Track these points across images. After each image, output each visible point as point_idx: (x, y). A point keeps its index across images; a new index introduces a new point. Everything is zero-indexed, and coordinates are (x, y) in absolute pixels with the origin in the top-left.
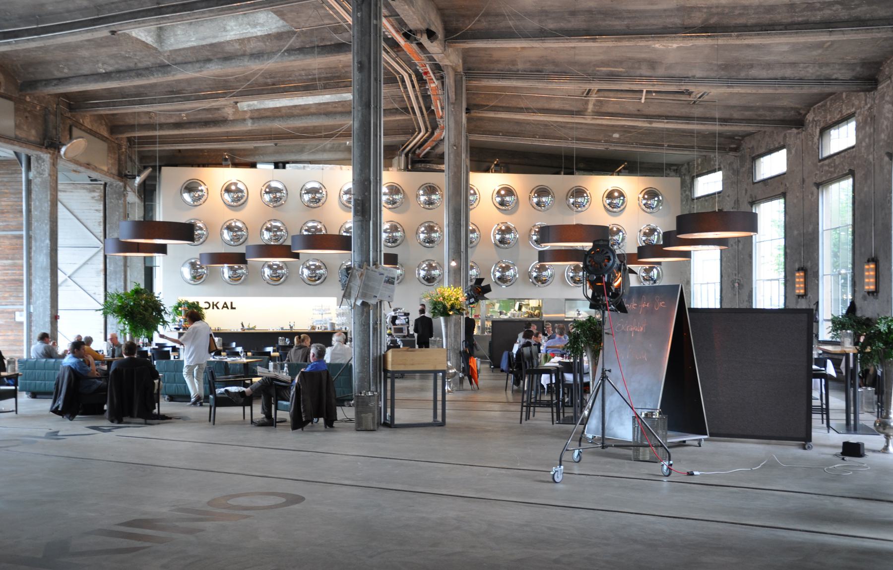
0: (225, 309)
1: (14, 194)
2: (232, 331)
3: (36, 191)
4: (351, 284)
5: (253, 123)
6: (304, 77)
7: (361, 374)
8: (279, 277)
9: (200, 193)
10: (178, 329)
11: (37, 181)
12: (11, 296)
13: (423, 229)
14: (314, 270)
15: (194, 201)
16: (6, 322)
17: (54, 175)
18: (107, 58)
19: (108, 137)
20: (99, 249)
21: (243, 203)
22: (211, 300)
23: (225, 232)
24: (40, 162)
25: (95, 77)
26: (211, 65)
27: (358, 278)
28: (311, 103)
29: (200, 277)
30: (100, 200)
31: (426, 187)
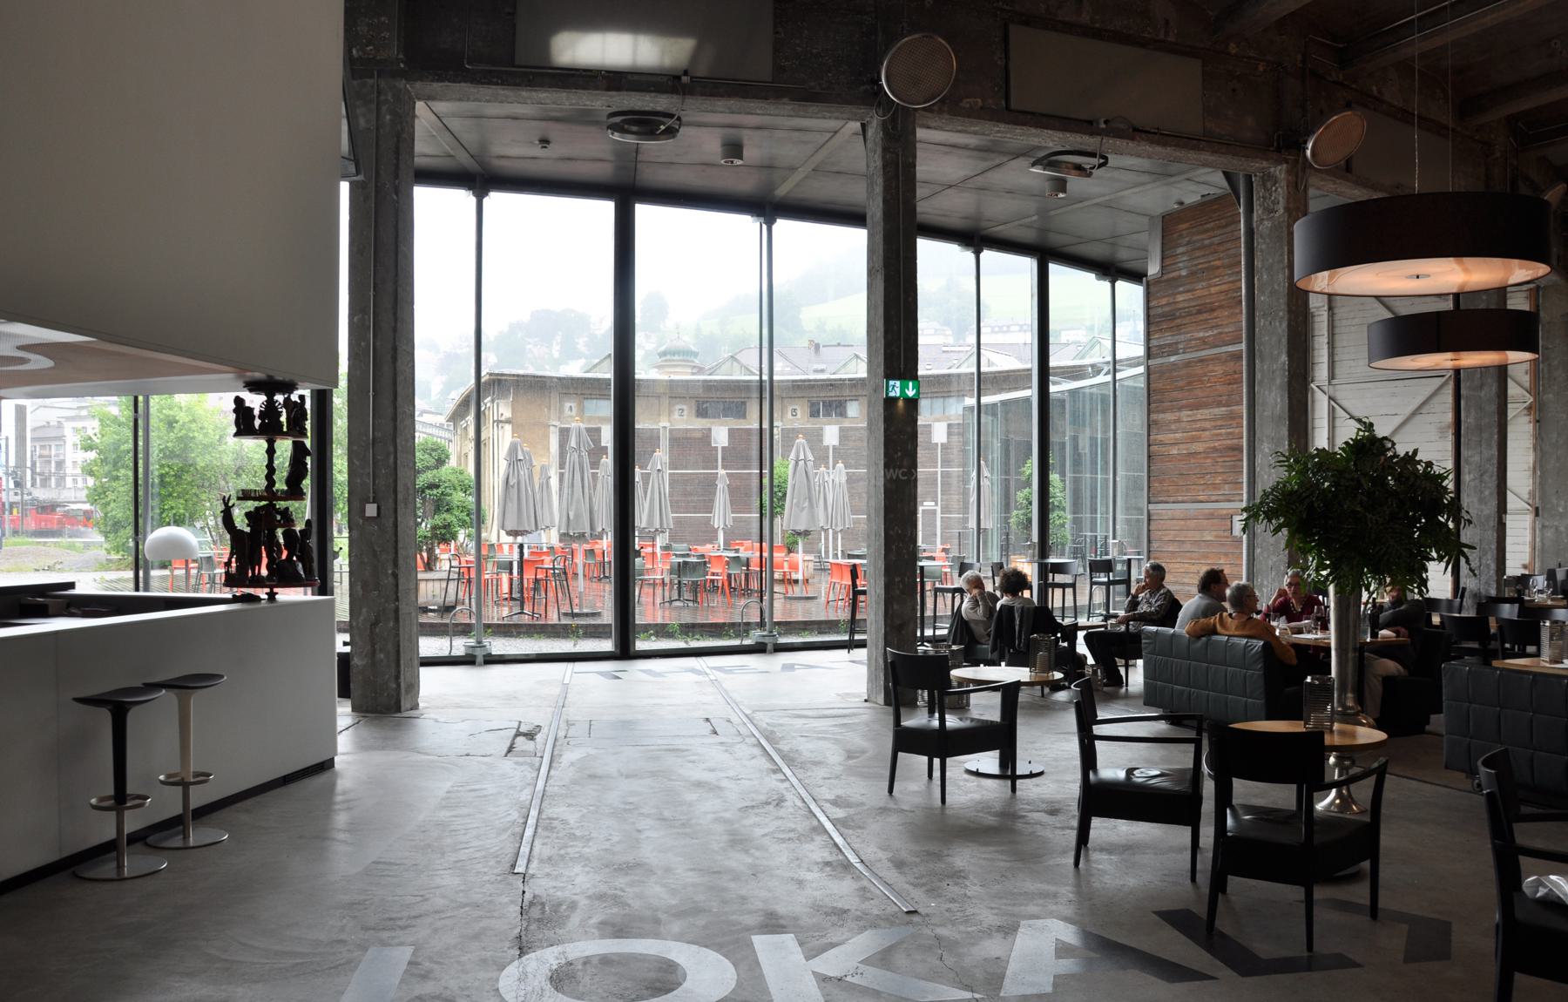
1: (1230, 266)
3: (1262, 251)
11: (1264, 227)
12: (1225, 482)
16: (1216, 537)
20: (1444, 379)
24: (1269, 185)
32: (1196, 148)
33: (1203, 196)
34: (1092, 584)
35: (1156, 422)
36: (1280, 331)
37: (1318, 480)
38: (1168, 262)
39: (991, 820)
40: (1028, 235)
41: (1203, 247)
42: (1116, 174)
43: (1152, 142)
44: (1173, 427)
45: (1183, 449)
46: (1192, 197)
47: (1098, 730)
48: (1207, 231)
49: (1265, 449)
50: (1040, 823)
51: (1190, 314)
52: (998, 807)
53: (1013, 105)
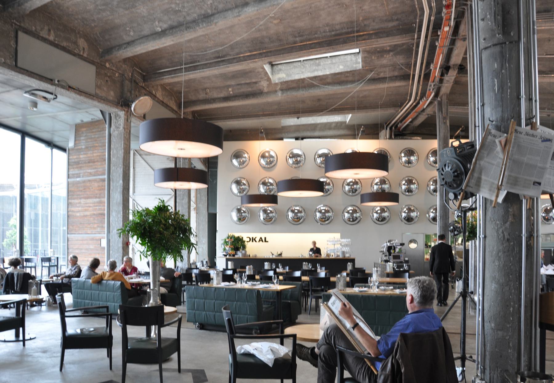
0: (261, 242)
1: (101, 146)
2: (266, 257)
3: (114, 142)
4: (482, 163)
5: (282, 94)
6: (328, 34)
7: (500, 333)
8: (299, 219)
9: (244, 159)
10: (225, 256)
12: (98, 227)
13: (404, 182)
14: (325, 213)
15: (240, 165)
17: (127, 129)
18: (162, 15)
19: (177, 110)
21: (274, 165)
22: (252, 235)
23: (261, 186)
24: (117, 118)
25: (154, 36)
26: (248, 8)
27: (499, 148)
28: (328, 73)
29: (244, 218)
30: (173, 160)
31: (406, 151)
32: (92, 99)
33: (92, 119)
34: (42, 267)
35: (71, 203)
36: (120, 171)
37: (147, 219)
38: (77, 142)
39: (15, 359)
40: (17, 125)
41: (91, 138)
42: (58, 105)
43: (76, 93)
44: (78, 205)
45: (82, 214)
46: (87, 118)
47: (66, 314)
48: (93, 132)
49: (113, 214)
50: (40, 357)
51: (85, 163)
52: (18, 353)
53: (19, 65)
